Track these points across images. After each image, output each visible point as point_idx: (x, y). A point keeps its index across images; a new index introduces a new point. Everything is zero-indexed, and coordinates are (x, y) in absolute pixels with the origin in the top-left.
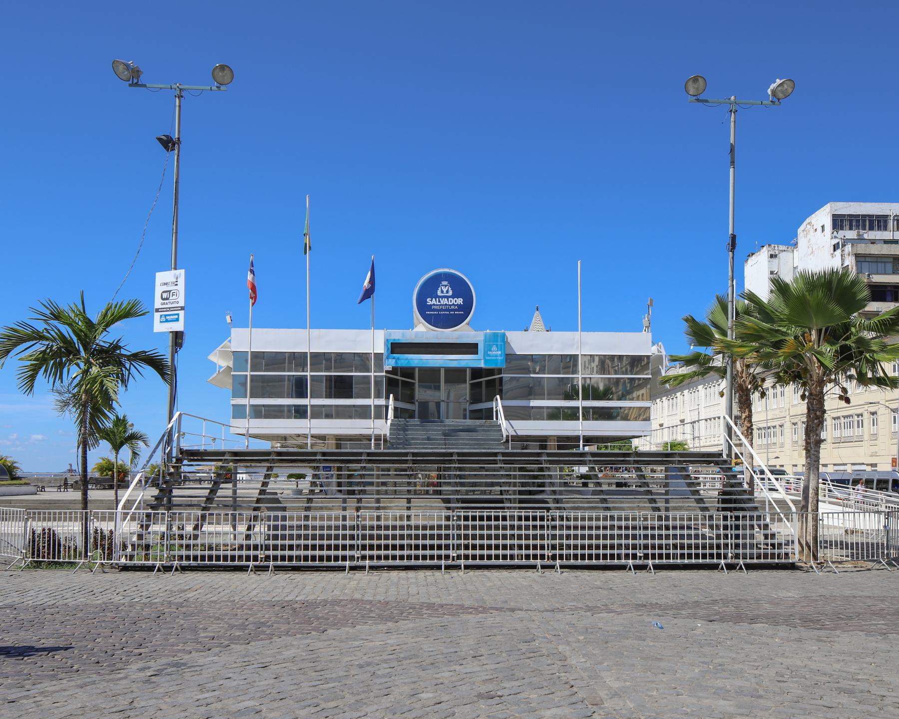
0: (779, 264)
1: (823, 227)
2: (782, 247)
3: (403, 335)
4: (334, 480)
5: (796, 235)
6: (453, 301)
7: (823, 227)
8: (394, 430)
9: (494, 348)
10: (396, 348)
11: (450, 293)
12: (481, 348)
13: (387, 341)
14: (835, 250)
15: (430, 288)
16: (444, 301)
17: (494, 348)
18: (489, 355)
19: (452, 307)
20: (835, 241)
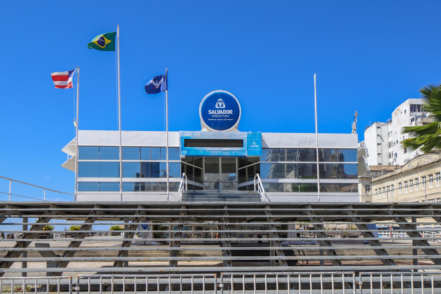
0: (381, 131)
1: (405, 111)
2: (382, 123)
3: (192, 134)
4: (151, 231)
5: (390, 117)
6: (226, 112)
7: (405, 111)
8: (185, 197)
9: (254, 143)
10: (188, 142)
11: (224, 106)
12: (245, 142)
13: (181, 138)
14: (412, 121)
15: (210, 103)
16: (220, 112)
17: (254, 143)
18: (251, 148)
19: (226, 116)
20: (412, 117)
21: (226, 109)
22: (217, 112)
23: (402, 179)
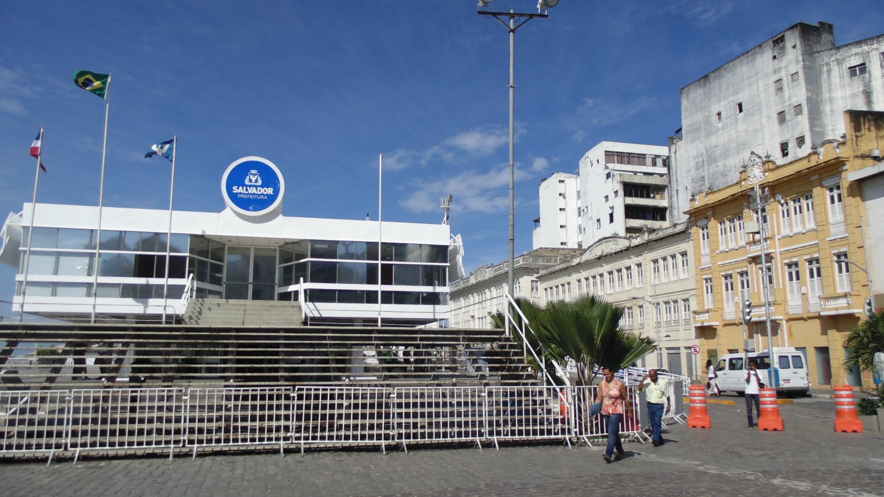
5: (578, 167)
11: (260, 183)
16: (252, 190)
21: (262, 186)
22: (247, 190)
23: (584, 274)
